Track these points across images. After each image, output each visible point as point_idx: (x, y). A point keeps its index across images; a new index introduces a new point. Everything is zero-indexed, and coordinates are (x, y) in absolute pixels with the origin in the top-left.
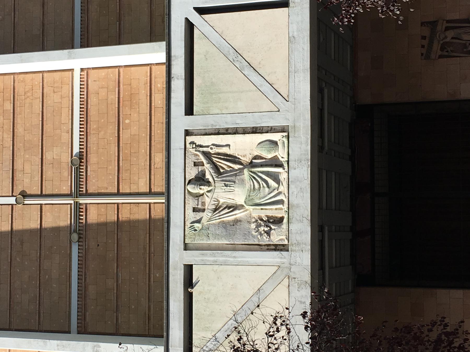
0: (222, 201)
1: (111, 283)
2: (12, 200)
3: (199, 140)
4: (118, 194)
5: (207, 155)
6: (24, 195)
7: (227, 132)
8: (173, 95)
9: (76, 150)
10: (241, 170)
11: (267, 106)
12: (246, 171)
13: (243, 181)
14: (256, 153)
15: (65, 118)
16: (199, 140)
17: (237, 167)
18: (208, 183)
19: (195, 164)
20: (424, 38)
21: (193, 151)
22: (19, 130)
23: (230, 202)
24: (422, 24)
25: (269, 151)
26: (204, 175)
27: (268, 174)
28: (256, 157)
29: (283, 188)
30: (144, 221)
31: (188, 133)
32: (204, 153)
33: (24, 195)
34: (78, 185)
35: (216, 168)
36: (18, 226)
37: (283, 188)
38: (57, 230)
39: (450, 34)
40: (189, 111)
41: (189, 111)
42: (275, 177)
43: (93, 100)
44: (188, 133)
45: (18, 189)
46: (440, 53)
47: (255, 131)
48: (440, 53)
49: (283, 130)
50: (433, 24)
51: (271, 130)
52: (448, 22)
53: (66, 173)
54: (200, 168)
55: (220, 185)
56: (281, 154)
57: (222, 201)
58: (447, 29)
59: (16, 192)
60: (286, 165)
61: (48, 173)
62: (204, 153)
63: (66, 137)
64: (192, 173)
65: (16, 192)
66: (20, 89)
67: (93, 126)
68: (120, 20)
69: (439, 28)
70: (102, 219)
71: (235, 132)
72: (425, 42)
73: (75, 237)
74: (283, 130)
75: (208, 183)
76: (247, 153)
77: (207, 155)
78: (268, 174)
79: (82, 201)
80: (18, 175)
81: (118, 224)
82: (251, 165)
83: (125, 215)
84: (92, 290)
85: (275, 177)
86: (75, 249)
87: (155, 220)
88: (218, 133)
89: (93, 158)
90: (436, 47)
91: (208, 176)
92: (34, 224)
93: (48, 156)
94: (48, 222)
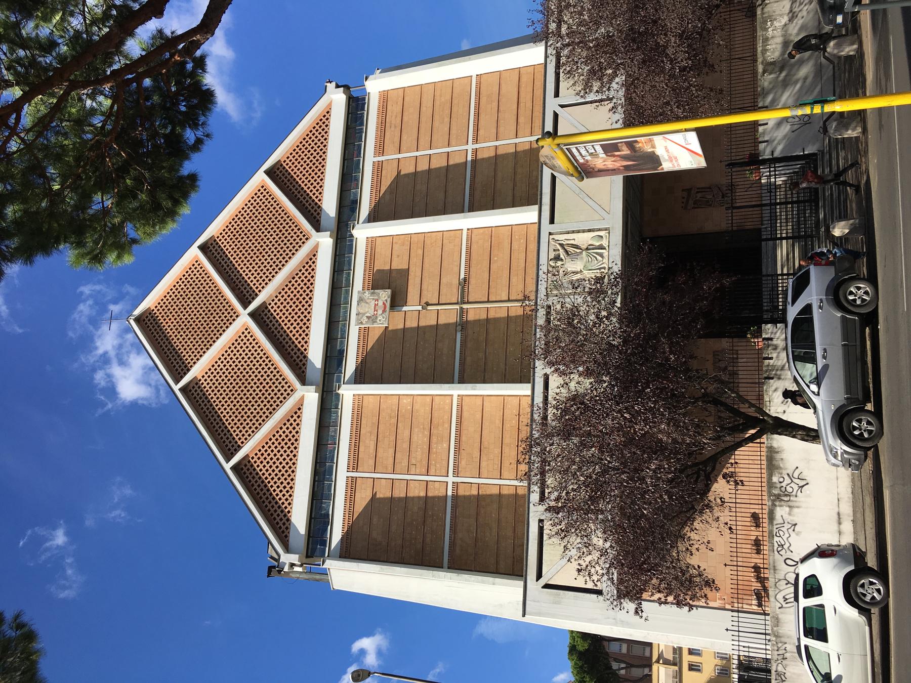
0: (569, 269)
1: (481, 355)
2: (420, 308)
3: (557, 237)
4: (488, 302)
5: (561, 245)
6: (428, 304)
7: (573, 232)
8: (542, 213)
9: (462, 276)
10: (581, 253)
11: (597, 217)
12: (584, 252)
13: (582, 258)
14: (590, 243)
15: (457, 258)
16: (557, 237)
17: (578, 251)
18: (562, 260)
19: (554, 250)
20: (683, 198)
21: (553, 243)
22: (426, 265)
23: (574, 270)
24: (683, 190)
25: (598, 241)
26: (559, 256)
27: (597, 253)
28: (590, 245)
29: (605, 260)
30: (504, 318)
31: (550, 234)
32: (560, 244)
33: (428, 304)
34: (463, 297)
35: (567, 252)
36: (422, 324)
37: (605, 260)
38: (447, 325)
39: (699, 195)
40: (552, 221)
41: (552, 221)
42: (601, 255)
43: (474, 247)
44: (550, 234)
45: (424, 301)
46: (693, 206)
47: (589, 231)
48: (693, 206)
49: (606, 229)
50: (689, 191)
51: (599, 230)
52: (698, 188)
53: (455, 291)
54: (557, 252)
55: (568, 259)
56: (605, 243)
57: (569, 269)
58: (698, 192)
59: (422, 303)
60: (607, 248)
61: (443, 291)
62: (560, 244)
63: (457, 269)
64: (552, 256)
65: (422, 303)
66: (428, 242)
67: (473, 262)
68: (494, 200)
69: (692, 192)
70: (477, 318)
71: (578, 232)
72: (684, 200)
73: (459, 328)
74: (606, 229)
75: (562, 260)
76: (585, 243)
77: (561, 245)
78: (597, 253)
79: (465, 306)
80: (424, 293)
81: (488, 320)
82: (587, 249)
83: (492, 315)
84: (469, 360)
85: (601, 255)
86: (459, 335)
87: (511, 317)
88: (568, 233)
89: (473, 281)
90: (691, 202)
91: (562, 256)
92: (433, 322)
93: (444, 281)
94: (442, 321)
